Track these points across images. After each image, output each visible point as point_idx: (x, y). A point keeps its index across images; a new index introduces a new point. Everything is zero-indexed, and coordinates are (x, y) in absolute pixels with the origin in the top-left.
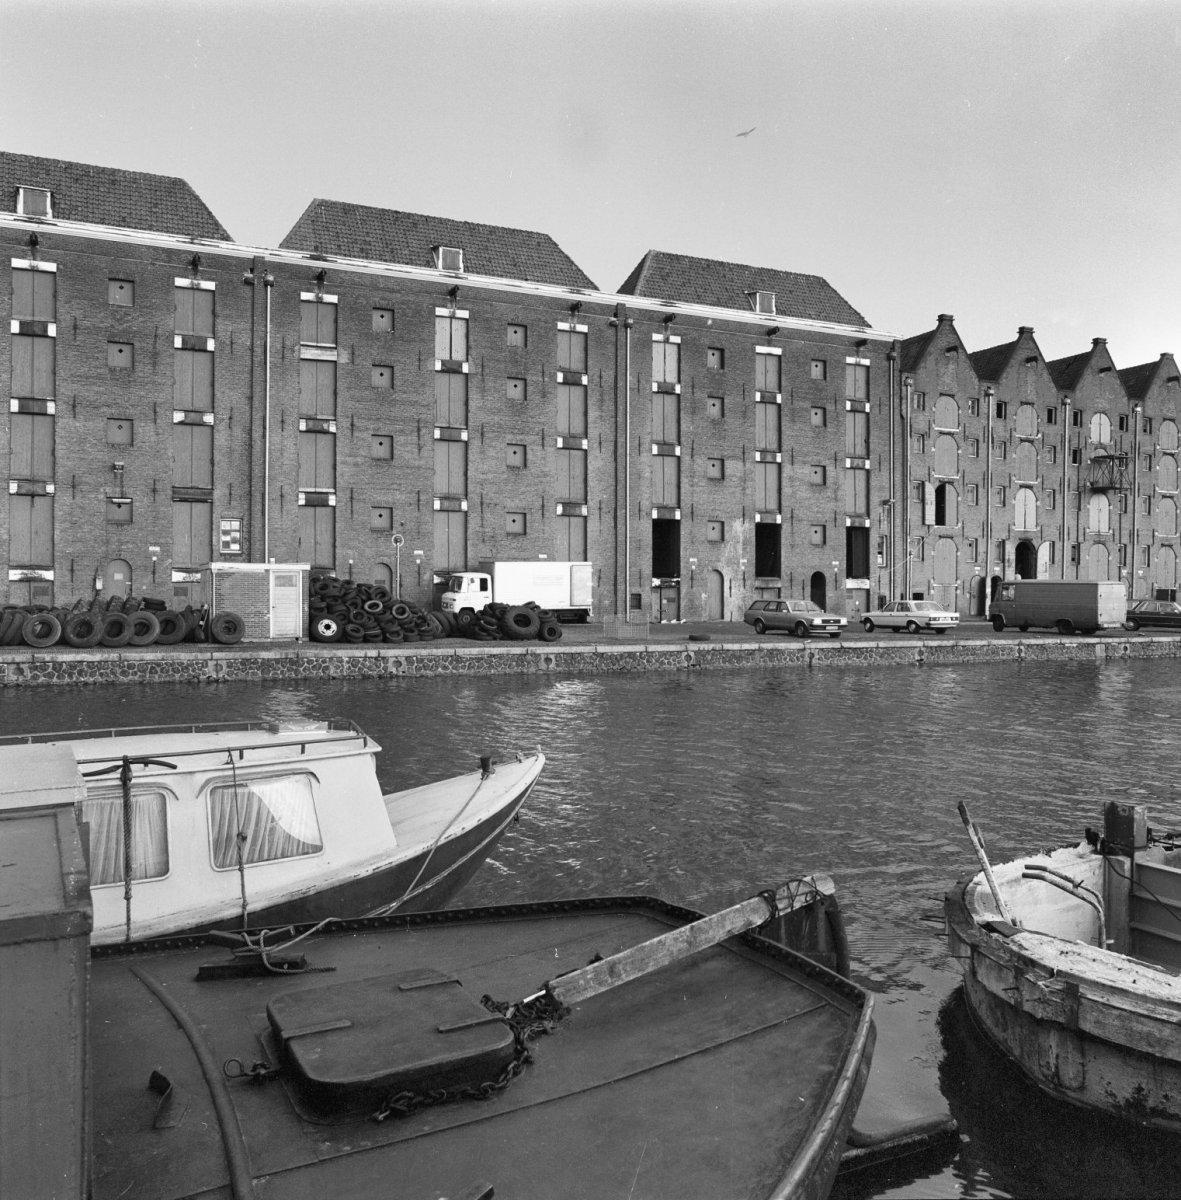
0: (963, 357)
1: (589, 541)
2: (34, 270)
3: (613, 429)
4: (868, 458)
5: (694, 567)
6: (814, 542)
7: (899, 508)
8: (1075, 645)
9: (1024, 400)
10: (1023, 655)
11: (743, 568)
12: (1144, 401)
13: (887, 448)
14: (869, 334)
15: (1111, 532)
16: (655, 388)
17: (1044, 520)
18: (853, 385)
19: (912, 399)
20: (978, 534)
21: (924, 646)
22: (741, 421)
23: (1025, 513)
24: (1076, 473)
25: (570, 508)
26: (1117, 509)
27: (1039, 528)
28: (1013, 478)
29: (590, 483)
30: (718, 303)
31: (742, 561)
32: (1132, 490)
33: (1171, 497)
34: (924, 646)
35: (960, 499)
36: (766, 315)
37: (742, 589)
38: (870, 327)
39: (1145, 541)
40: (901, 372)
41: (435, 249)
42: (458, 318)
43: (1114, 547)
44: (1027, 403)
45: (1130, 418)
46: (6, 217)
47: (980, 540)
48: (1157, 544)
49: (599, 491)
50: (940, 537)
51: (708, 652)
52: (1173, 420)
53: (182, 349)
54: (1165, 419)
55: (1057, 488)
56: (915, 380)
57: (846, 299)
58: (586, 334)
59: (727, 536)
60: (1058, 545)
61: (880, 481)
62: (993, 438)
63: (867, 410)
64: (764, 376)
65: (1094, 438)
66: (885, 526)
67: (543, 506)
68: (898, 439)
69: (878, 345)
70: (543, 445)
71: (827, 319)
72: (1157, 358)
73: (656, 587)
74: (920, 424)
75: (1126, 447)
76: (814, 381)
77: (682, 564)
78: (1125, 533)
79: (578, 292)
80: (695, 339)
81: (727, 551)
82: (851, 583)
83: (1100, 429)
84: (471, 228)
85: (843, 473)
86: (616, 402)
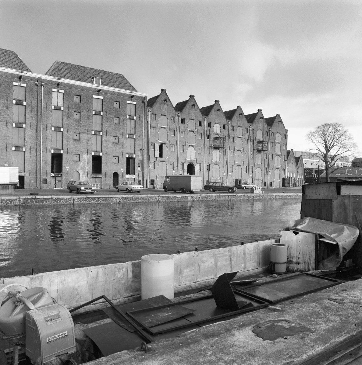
0: (243, 116)
1: (25, 160)
2: (131, 104)
3: (36, 121)
4: (135, 135)
5: (68, 170)
6: (115, 162)
7: (146, 151)
8: (180, 197)
9: (191, 118)
10: (160, 200)
11: (87, 170)
12: (231, 121)
13: (142, 132)
14: (135, 94)
15: (220, 161)
16: (53, 107)
17: (197, 157)
18: (130, 110)
19: (151, 116)
20: (174, 160)
21: (121, 197)
22: (87, 120)
23: (191, 155)
24: (209, 142)
25: (18, 148)
26: (222, 154)
27: (196, 159)
28: (187, 143)
29: (26, 140)
30: (80, 80)
31: (87, 168)
32: (227, 148)
33: (240, 151)
34: (121, 197)
35: (168, 149)
36: (97, 85)
37: (87, 177)
38: (137, 91)
39: (231, 164)
40: (147, 107)
41: (93, 78)
42: (60, 93)
43: (221, 166)
44: (192, 119)
45: (227, 125)
46: (127, 91)
47: (175, 163)
48: (236, 165)
49: (30, 143)
50: (237, 165)
51: (29, 199)
52: (241, 127)
53: (94, 114)
54: (238, 127)
55: (202, 147)
56: (152, 110)
57: (130, 82)
58: (135, 105)
59: (81, 160)
60: (202, 165)
61: (139, 143)
62: (180, 130)
63: (135, 119)
64: (96, 106)
65: (215, 131)
66: (141, 158)
67: (7, 147)
68: (146, 129)
69: (138, 98)
70: (7, 126)
71: (121, 88)
72: (275, 115)
73: (53, 176)
74: (154, 124)
75: (226, 135)
76: (115, 108)
77: (63, 169)
78: (225, 161)
79: (22, 72)
80: (69, 92)
81: (81, 164)
82: (128, 176)
83: (217, 129)
84: (104, 72)
85: (125, 139)
86: (37, 112)
